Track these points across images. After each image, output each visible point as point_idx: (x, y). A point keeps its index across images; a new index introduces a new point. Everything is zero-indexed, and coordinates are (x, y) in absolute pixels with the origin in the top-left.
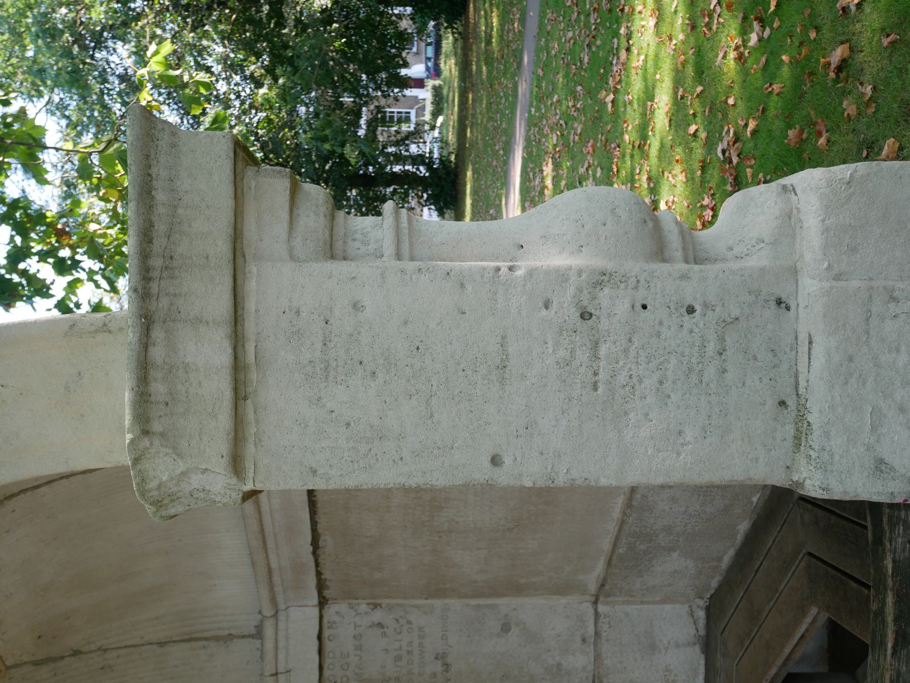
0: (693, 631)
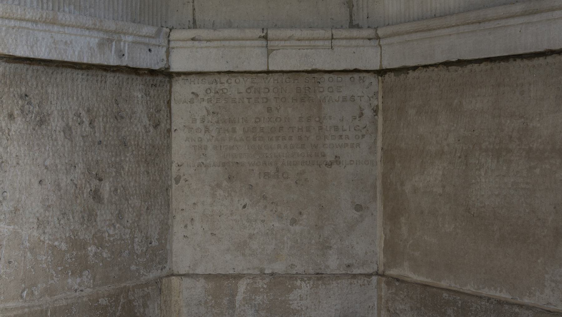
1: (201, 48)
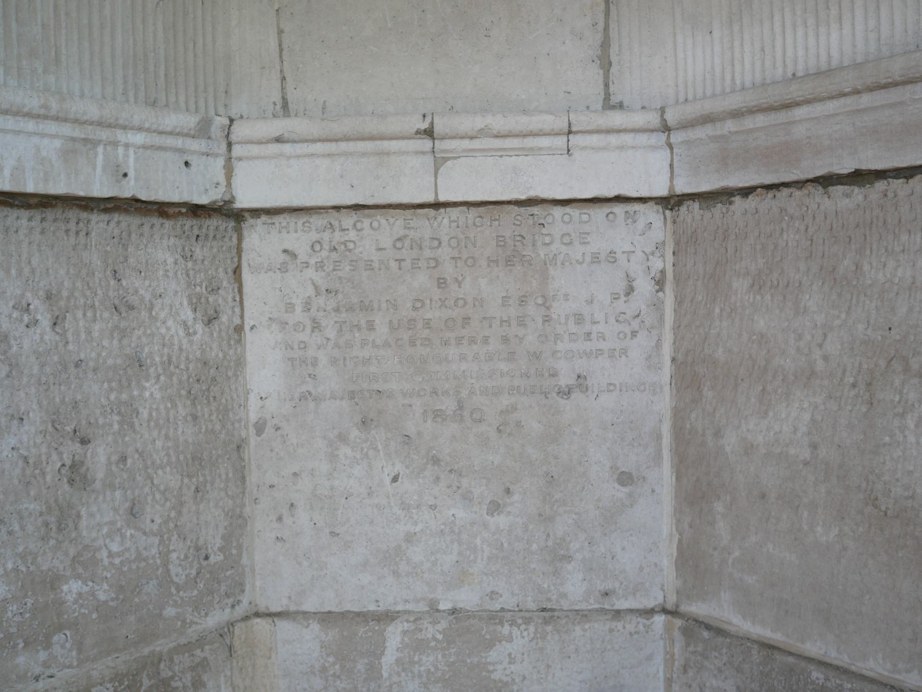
1: (298, 157)
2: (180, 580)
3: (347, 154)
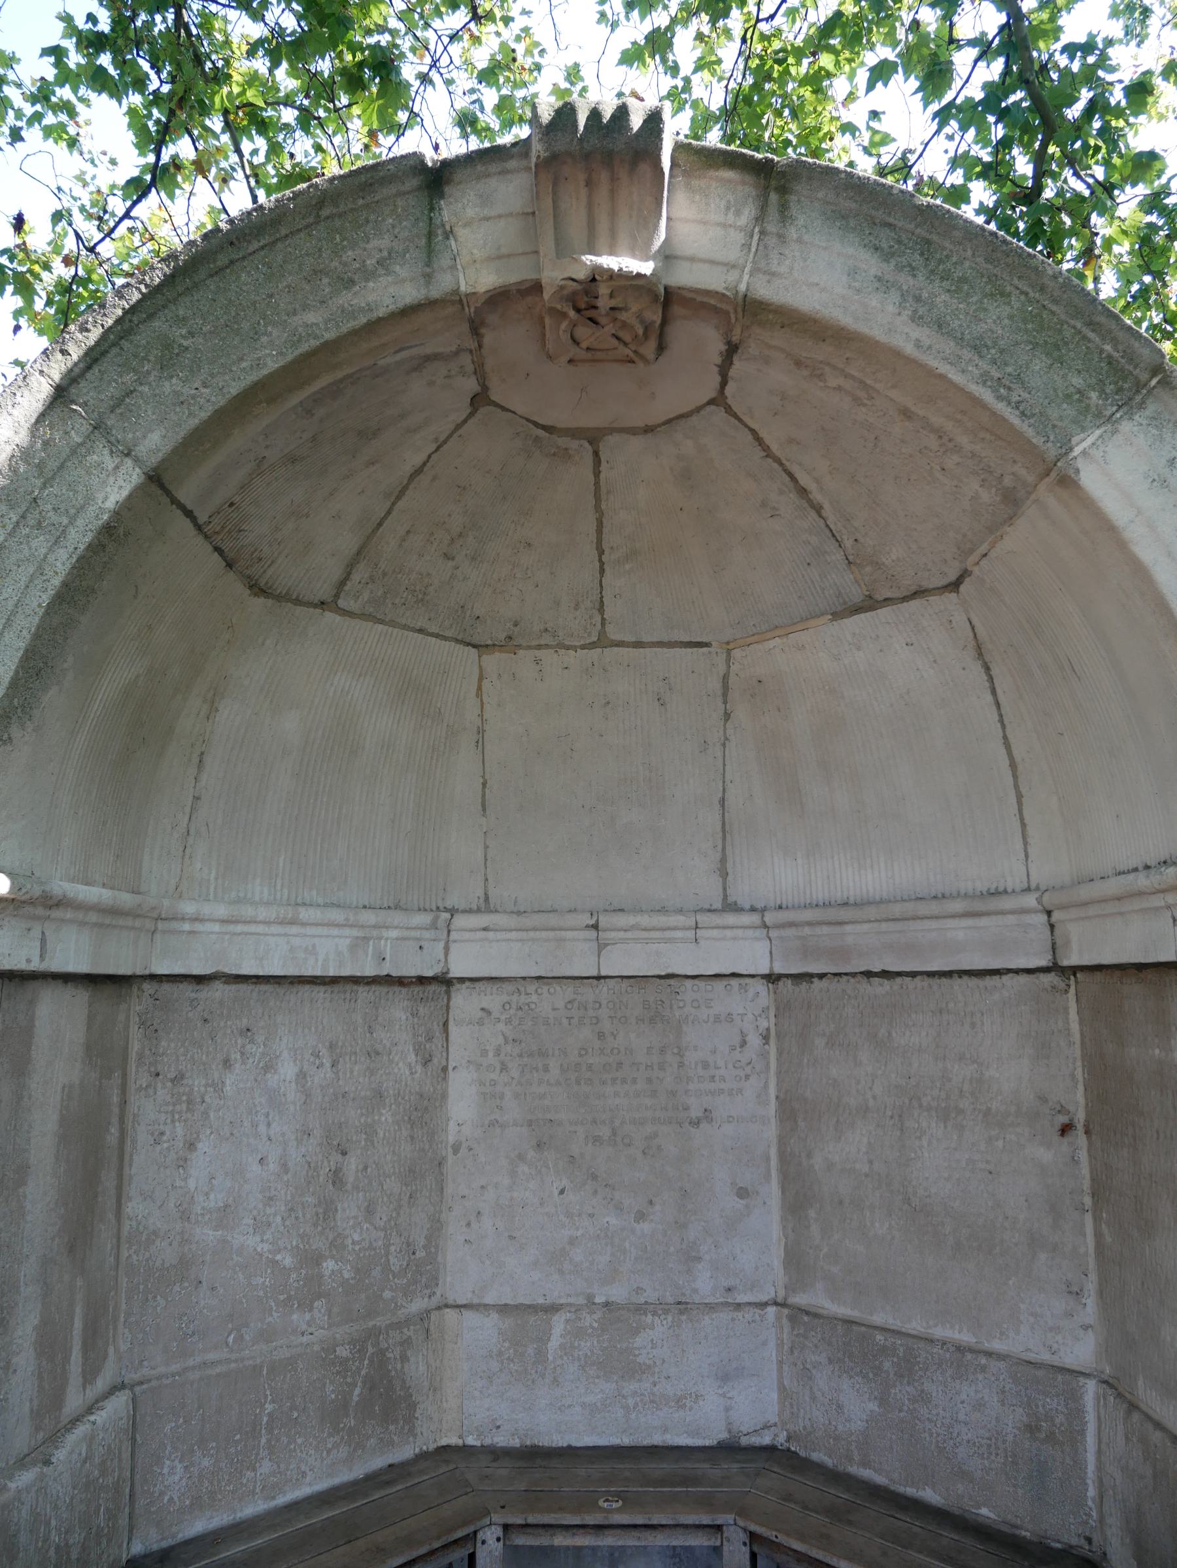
0: (744, 1430)
2: (396, 1269)
3: (533, 940)
